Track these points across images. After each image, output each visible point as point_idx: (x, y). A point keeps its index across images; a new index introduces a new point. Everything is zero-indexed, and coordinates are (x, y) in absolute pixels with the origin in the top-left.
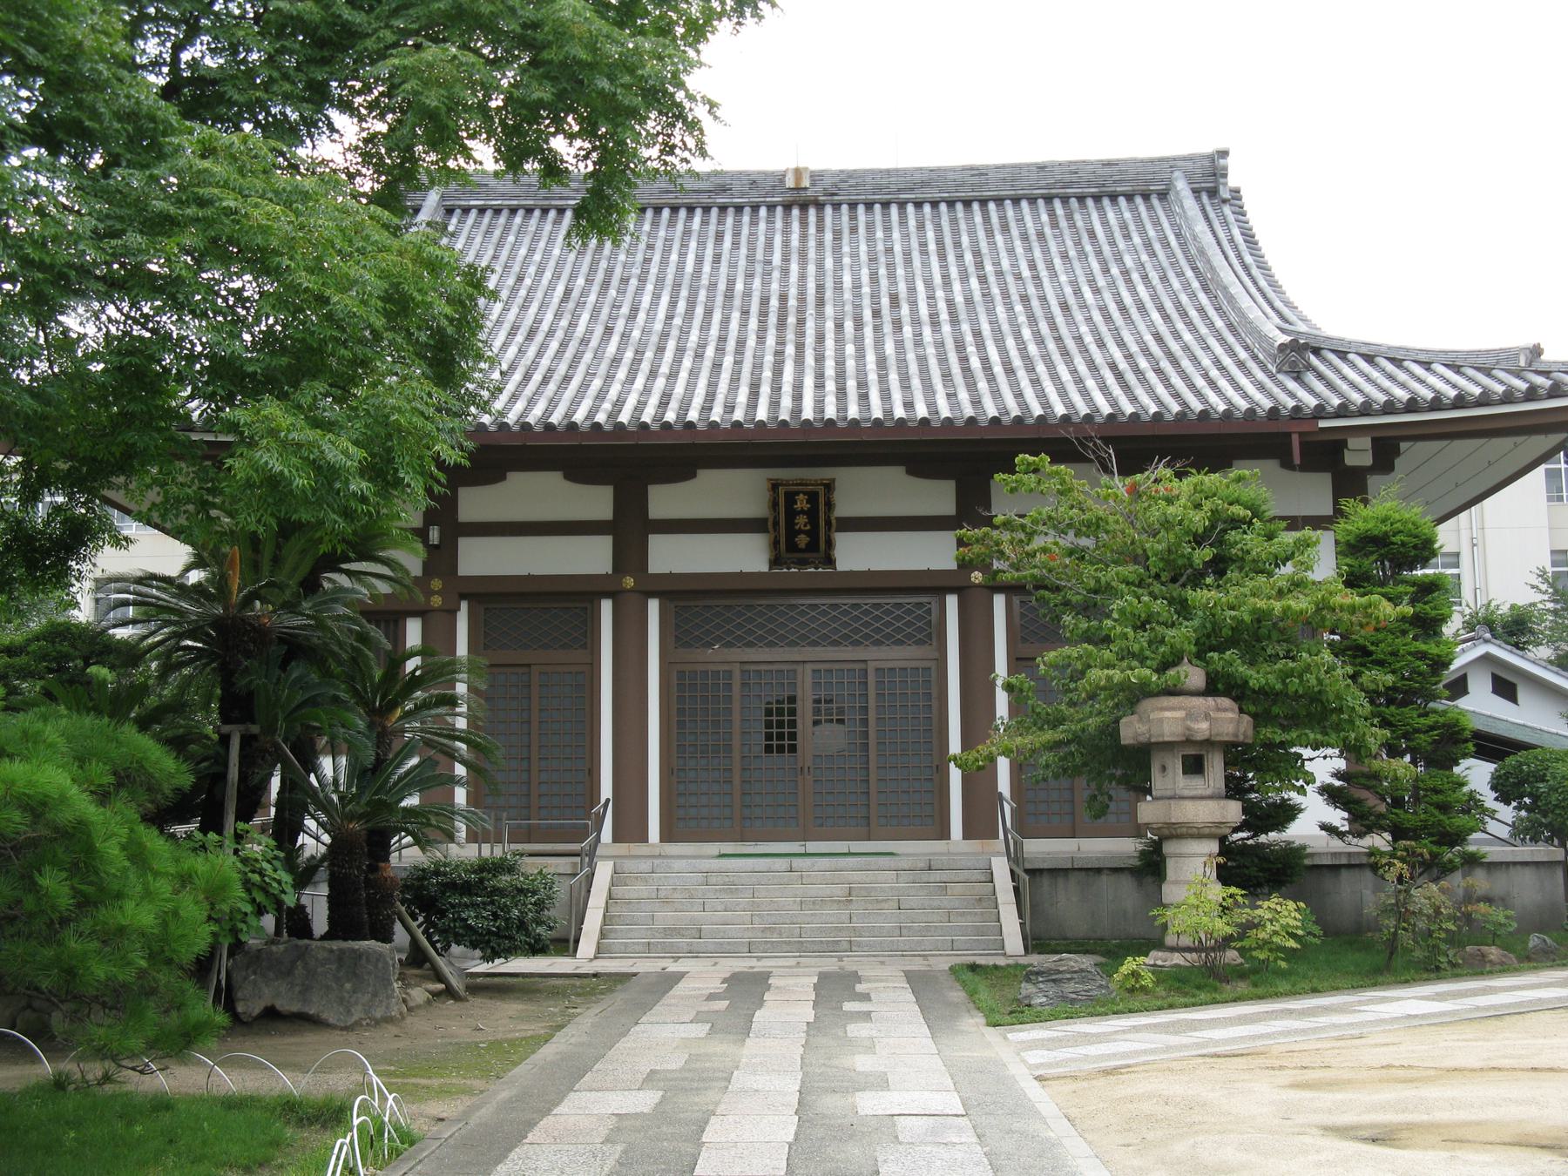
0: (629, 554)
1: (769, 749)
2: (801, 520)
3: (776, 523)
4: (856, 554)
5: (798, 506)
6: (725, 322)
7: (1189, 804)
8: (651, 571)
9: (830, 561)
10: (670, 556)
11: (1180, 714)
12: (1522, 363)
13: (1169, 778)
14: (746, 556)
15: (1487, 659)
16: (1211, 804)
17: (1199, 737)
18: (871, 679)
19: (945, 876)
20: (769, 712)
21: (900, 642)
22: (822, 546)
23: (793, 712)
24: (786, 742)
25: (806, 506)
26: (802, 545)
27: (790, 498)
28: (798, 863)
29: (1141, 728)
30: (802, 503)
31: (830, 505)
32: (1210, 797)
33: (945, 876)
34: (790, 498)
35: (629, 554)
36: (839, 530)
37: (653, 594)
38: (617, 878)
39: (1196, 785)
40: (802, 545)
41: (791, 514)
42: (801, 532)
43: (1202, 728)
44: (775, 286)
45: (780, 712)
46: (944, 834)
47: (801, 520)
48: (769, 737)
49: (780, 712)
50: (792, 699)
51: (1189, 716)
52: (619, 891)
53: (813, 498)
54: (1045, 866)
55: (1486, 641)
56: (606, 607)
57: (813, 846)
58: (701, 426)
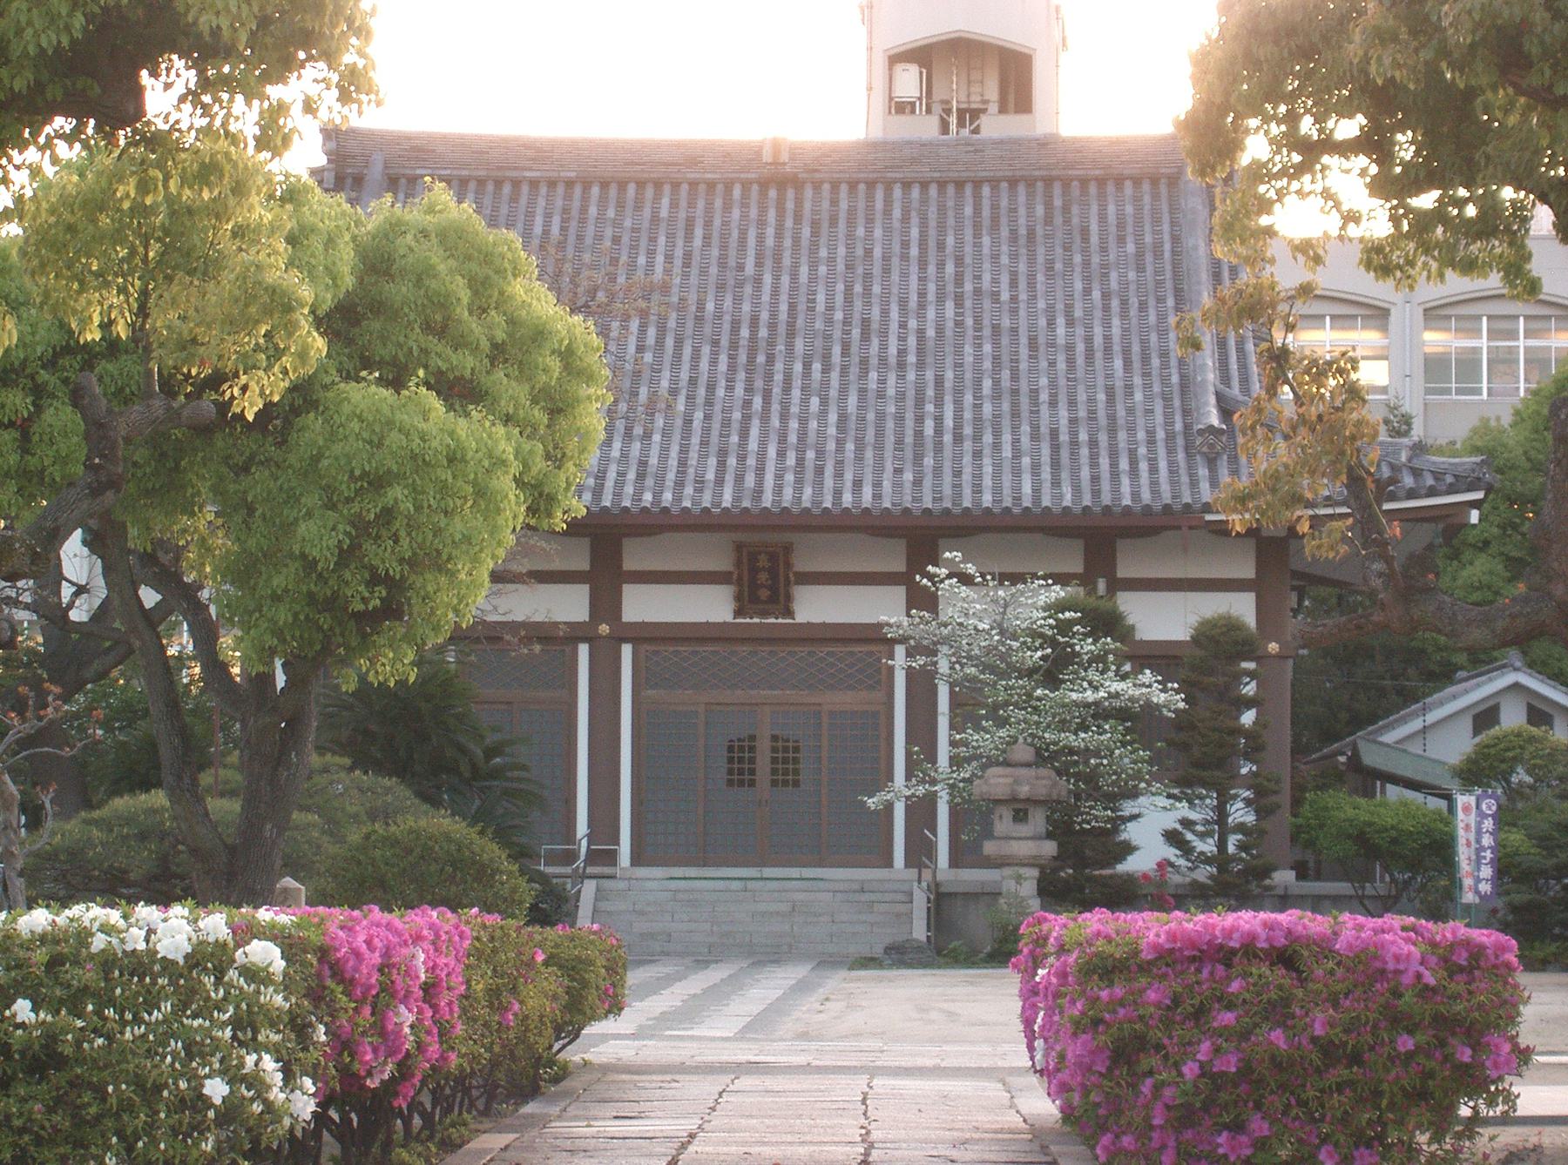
0: (605, 603)
1: (730, 783)
2: (763, 577)
3: (740, 579)
4: (817, 607)
5: (760, 564)
6: (696, 357)
7: (1013, 843)
8: (624, 620)
9: (789, 613)
10: (643, 605)
11: (1010, 780)
12: (1404, 459)
13: (1003, 823)
14: (711, 606)
15: (1516, 687)
16: (1030, 843)
17: (1022, 796)
18: (825, 720)
19: (873, 897)
20: (730, 749)
21: (851, 688)
22: (782, 599)
23: (752, 749)
24: (746, 777)
25: (767, 565)
26: (763, 598)
27: (753, 558)
28: (750, 885)
29: (985, 789)
30: (763, 561)
31: (788, 565)
32: (1031, 838)
33: (873, 897)
34: (753, 558)
35: (605, 603)
36: (798, 583)
37: (626, 640)
38: (600, 895)
39: (1024, 830)
40: (763, 598)
41: (754, 571)
42: (762, 586)
43: (1024, 790)
44: (746, 307)
45: (741, 749)
46: (889, 863)
47: (763, 577)
48: (730, 772)
49: (741, 749)
50: (752, 738)
51: (1017, 781)
52: (603, 905)
53: (773, 557)
54: (961, 890)
55: (1516, 669)
56: (583, 650)
57: (768, 872)
58: (675, 510)
